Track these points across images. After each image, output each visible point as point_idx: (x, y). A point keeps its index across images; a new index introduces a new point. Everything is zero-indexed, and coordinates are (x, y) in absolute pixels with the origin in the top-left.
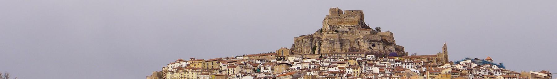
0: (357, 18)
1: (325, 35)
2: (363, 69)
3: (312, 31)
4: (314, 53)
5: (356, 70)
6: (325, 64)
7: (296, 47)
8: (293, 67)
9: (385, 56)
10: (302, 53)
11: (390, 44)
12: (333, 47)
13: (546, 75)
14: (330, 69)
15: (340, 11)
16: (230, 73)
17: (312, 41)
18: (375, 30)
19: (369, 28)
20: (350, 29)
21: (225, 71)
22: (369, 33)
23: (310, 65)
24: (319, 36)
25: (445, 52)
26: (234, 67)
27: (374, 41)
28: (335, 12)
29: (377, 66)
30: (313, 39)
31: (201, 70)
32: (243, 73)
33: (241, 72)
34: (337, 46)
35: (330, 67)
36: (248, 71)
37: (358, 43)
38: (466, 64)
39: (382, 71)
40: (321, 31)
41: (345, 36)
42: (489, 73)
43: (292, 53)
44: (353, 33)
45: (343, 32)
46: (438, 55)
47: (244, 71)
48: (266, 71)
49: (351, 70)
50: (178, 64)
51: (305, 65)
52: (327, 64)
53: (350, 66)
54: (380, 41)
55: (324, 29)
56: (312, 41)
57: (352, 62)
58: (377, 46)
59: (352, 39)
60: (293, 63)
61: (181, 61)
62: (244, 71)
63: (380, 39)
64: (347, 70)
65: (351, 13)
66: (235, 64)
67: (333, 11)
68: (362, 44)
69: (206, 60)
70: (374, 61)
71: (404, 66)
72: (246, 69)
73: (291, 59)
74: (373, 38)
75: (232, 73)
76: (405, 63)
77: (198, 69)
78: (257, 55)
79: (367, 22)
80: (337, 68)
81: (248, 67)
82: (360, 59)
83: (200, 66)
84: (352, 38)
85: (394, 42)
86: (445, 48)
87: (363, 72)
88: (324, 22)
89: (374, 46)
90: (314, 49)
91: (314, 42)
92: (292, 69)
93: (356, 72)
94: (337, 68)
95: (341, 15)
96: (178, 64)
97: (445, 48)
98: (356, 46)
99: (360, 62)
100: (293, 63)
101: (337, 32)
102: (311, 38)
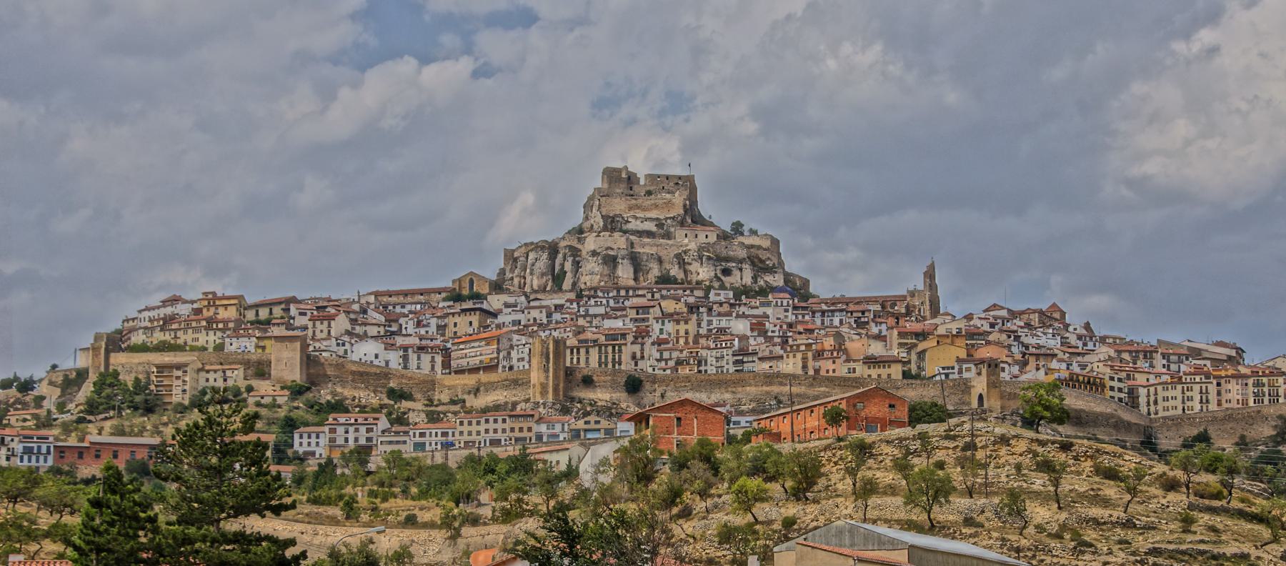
0: (679, 198)
1: (591, 243)
2: (704, 324)
3: (555, 232)
4: (560, 289)
5: (682, 328)
6: (592, 311)
7: (509, 275)
8: (501, 319)
9: (763, 292)
10: (527, 289)
11: (771, 270)
12: (612, 275)
13: (1233, 353)
14: (608, 324)
15: (631, 179)
16: (319, 335)
17: (553, 257)
18: (728, 229)
19: (712, 224)
20: (660, 225)
21: (306, 328)
22: (713, 238)
23: (549, 315)
24: (575, 244)
25: (932, 287)
26: (331, 318)
27: (728, 259)
28: (620, 180)
29: (744, 316)
30: (557, 252)
31: (231, 325)
32: (358, 336)
33: (348, 333)
34: (625, 273)
35: (605, 316)
36: (373, 331)
37: (682, 263)
38: (995, 318)
39: (759, 327)
40: (580, 231)
41: (646, 248)
42: (1062, 344)
43: (497, 287)
44: (668, 236)
45: (640, 234)
46: (912, 294)
47: (359, 330)
48: (423, 331)
49: (670, 327)
50: (169, 310)
51: (535, 314)
52: (601, 310)
53: (665, 316)
54: (741, 261)
55: (587, 225)
56: (553, 257)
57: (669, 306)
58: (736, 273)
59: (669, 253)
60: (500, 311)
61: (175, 300)
62: (359, 330)
63: (742, 253)
64: (657, 327)
65: (661, 183)
66: (333, 311)
67: (612, 175)
68: (695, 267)
69: (250, 300)
70: (732, 305)
71: (818, 321)
72: (365, 324)
73: (495, 302)
74: (722, 250)
75: (324, 335)
76: (823, 312)
77: (225, 322)
78: (398, 293)
79: (705, 208)
80: (627, 320)
81: (371, 321)
82: (691, 300)
83: (232, 313)
84: (668, 250)
85: (781, 264)
86: (930, 275)
87: (703, 331)
88: (588, 207)
89: (727, 272)
90: (558, 279)
91: (558, 262)
92: (498, 327)
93: (682, 333)
94: (627, 320)
95: (635, 187)
96: (169, 310)
97: (930, 275)
98: (675, 271)
99: (692, 309)
100: (500, 311)
101: (625, 232)
102: (552, 249)
